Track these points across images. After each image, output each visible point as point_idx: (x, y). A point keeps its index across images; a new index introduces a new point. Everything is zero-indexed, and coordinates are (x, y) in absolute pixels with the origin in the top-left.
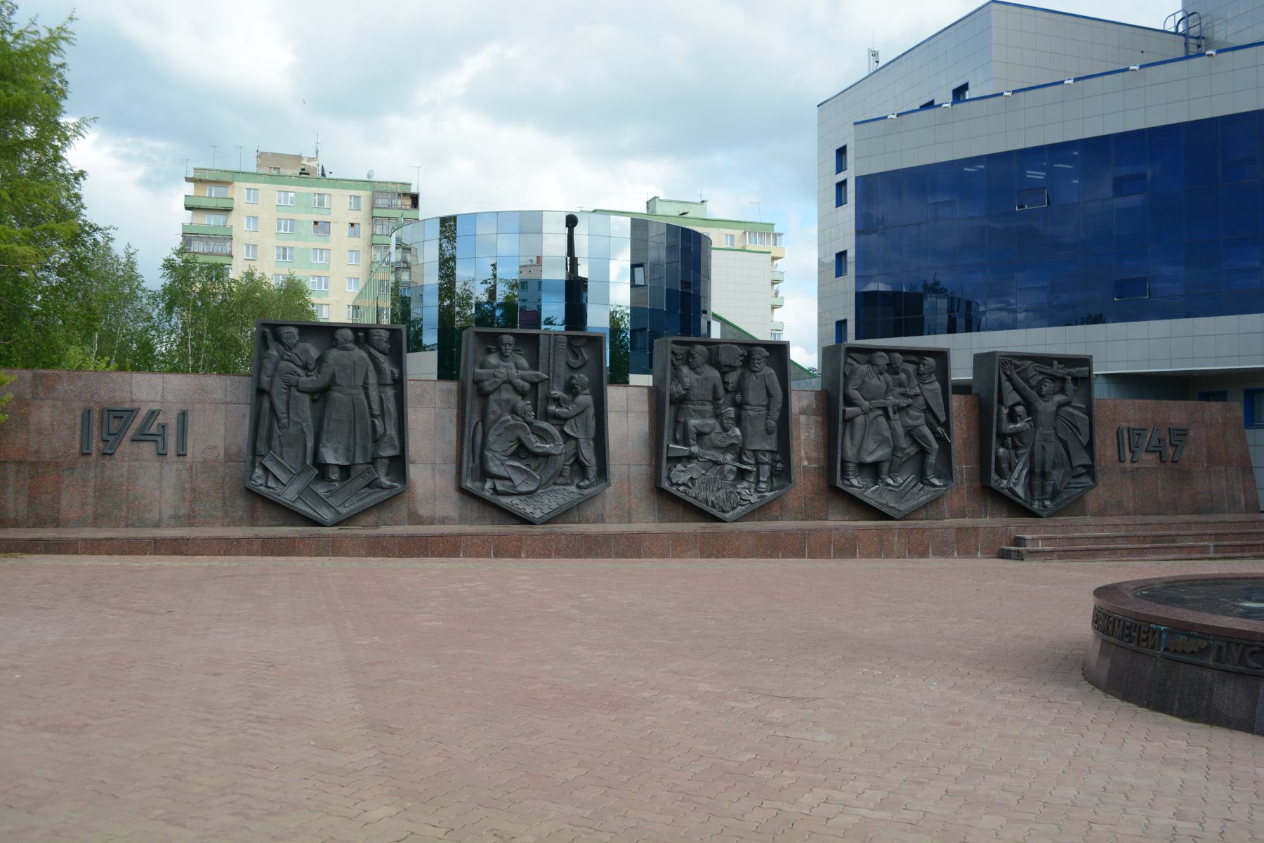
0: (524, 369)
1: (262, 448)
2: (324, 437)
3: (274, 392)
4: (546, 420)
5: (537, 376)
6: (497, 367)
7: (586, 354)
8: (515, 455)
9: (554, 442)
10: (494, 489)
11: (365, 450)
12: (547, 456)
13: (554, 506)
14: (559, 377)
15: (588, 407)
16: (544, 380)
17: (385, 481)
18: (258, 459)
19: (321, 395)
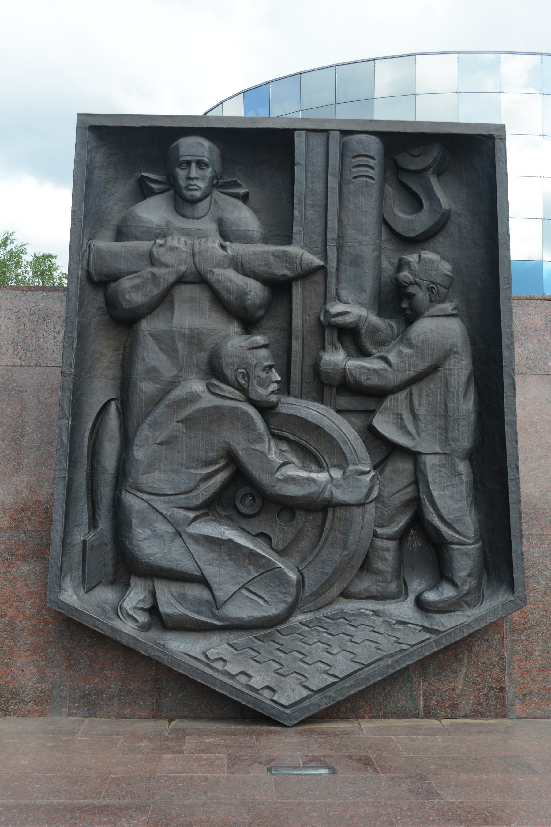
0: (245, 238)
4: (320, 400)
5: (286, 258)
6: (164, 233)
7: (445, 196)
8: (215, 506)
9: (343, 465)
10: (153, 610)
12: (321, 507)
13: (343, 665)
14: (356, 262)
15: (448, 354)
16: (308, 274)
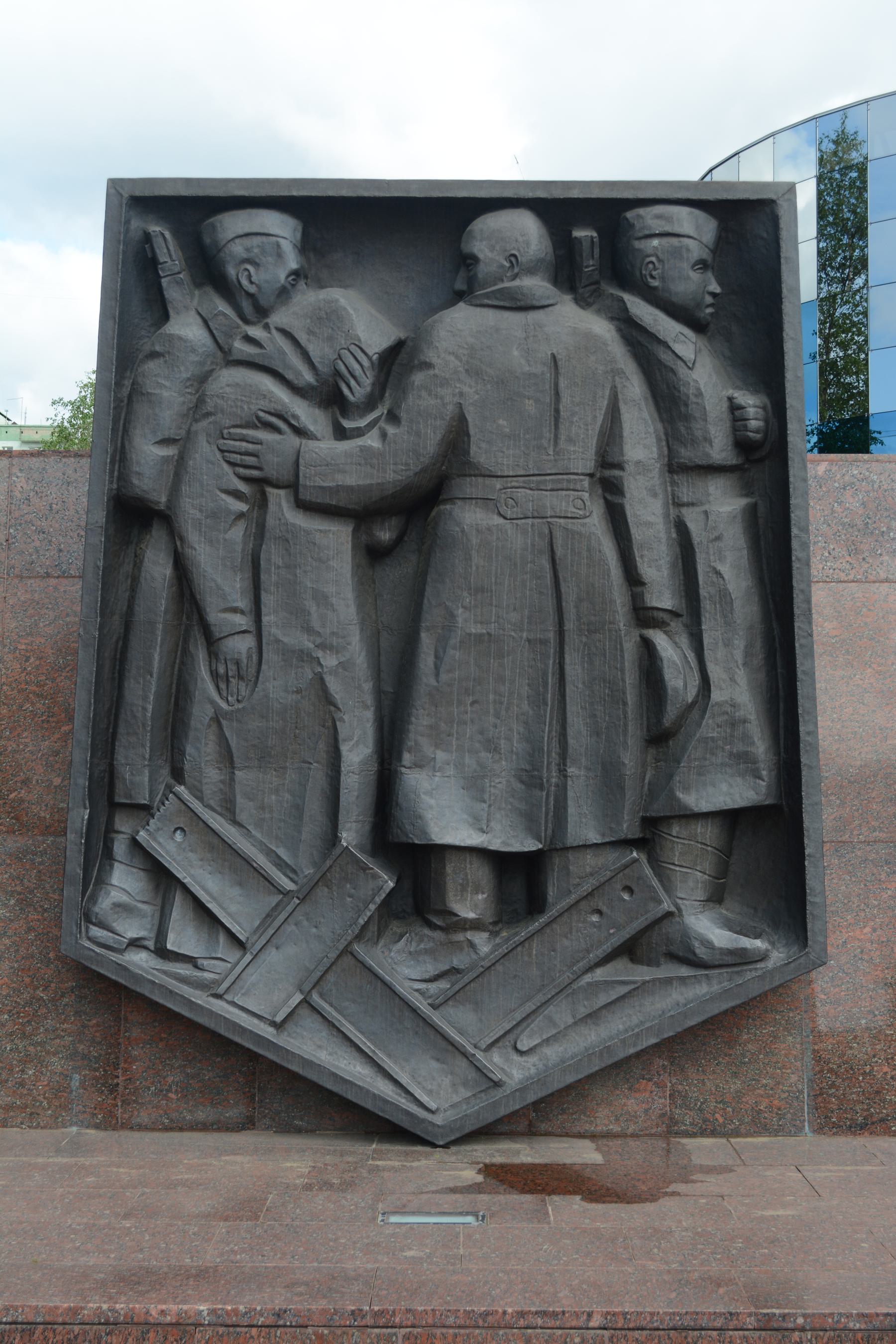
1: (138, 774)
2: (420, 721)
3: (190, 512)
11: (609, 779)
17: (710, 930)
18: (124, 825)
19: (403, 524)
